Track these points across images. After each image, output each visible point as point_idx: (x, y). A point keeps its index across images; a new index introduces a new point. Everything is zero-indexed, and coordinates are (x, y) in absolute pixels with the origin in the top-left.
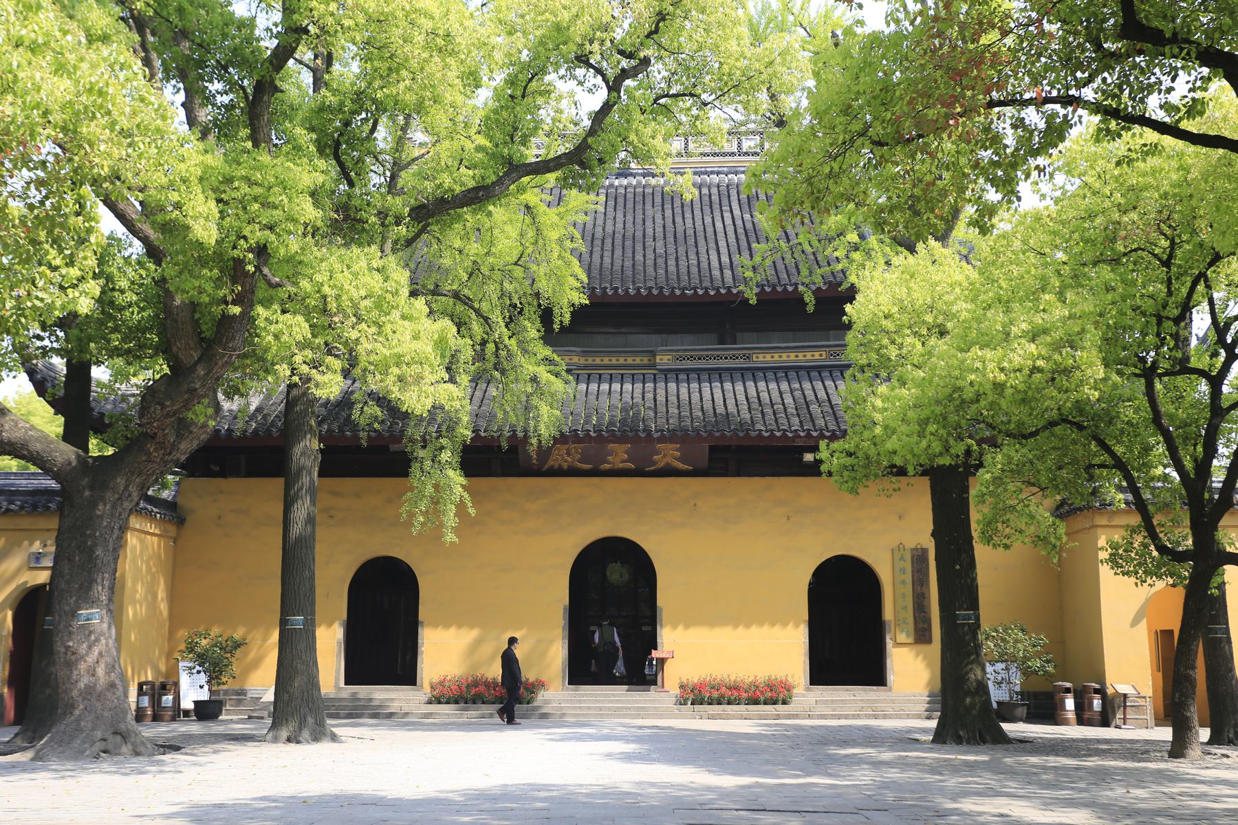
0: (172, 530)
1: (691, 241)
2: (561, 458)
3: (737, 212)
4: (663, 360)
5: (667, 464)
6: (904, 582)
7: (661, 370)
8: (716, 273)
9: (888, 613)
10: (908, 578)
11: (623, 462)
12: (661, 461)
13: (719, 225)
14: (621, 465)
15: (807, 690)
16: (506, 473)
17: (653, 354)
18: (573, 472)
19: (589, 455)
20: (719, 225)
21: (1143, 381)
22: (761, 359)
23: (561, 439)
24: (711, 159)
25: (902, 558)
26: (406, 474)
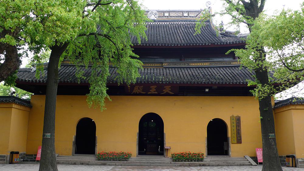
0: (28, 109)
1: (172, 35)
2: (136, 90)
3: (183, 29)
4: (165, 65)
5: (167, 92)
6: (234, 126)
7: (165, 68)
8: (180, 41)
9: (229, 135)
10: (235, 124)
11: (154, 91)
12: (165, 91)
13: (179, 32)
14: (154, 93)
15: (207, 157)
16: (121, 94)
17: (162, 63)
18: (140, 94)
19: (146, 89)
20: (179, 32)
21: (14, 155)
22: (192, 65)
23: (137, 84)
24: (176, 18)
25: (233, 119)
26: (88, 92)
